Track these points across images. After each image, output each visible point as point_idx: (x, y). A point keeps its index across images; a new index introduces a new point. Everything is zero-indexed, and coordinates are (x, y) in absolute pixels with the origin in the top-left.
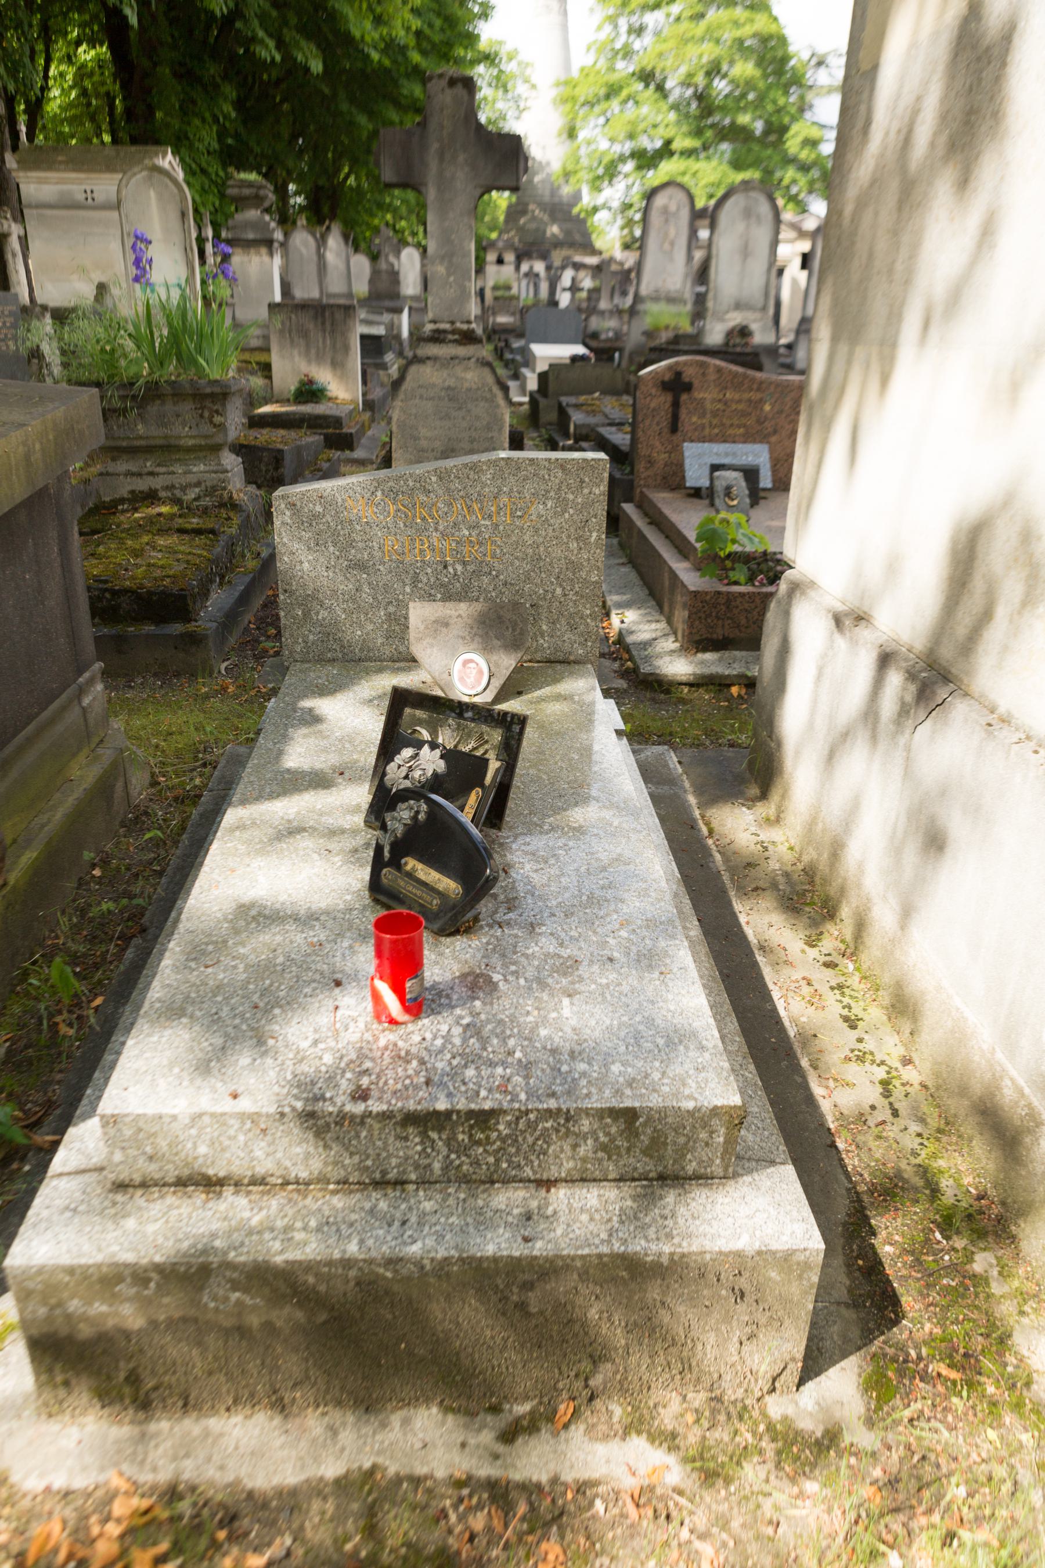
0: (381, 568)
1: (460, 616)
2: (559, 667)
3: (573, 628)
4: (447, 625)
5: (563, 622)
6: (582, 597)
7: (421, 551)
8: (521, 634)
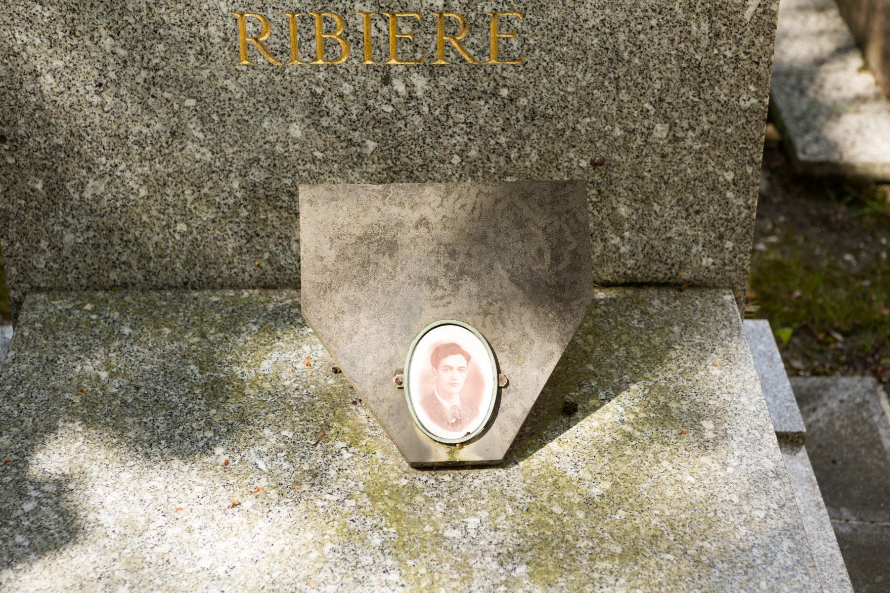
0: (231, 84)
1: (423, 222)
2: (656, 302)
3: (689, 212)
4: (391, 247)
5: (669, 198)
6: (716, 142)
7: (326, 46)
8: (574, 268)
